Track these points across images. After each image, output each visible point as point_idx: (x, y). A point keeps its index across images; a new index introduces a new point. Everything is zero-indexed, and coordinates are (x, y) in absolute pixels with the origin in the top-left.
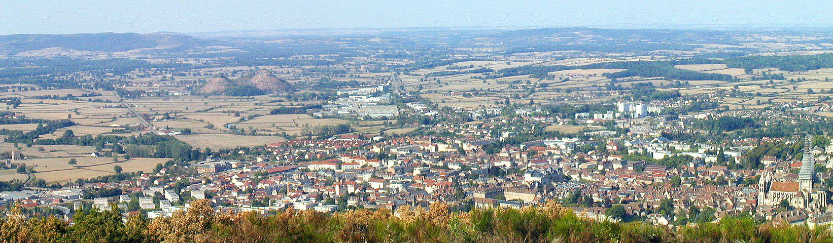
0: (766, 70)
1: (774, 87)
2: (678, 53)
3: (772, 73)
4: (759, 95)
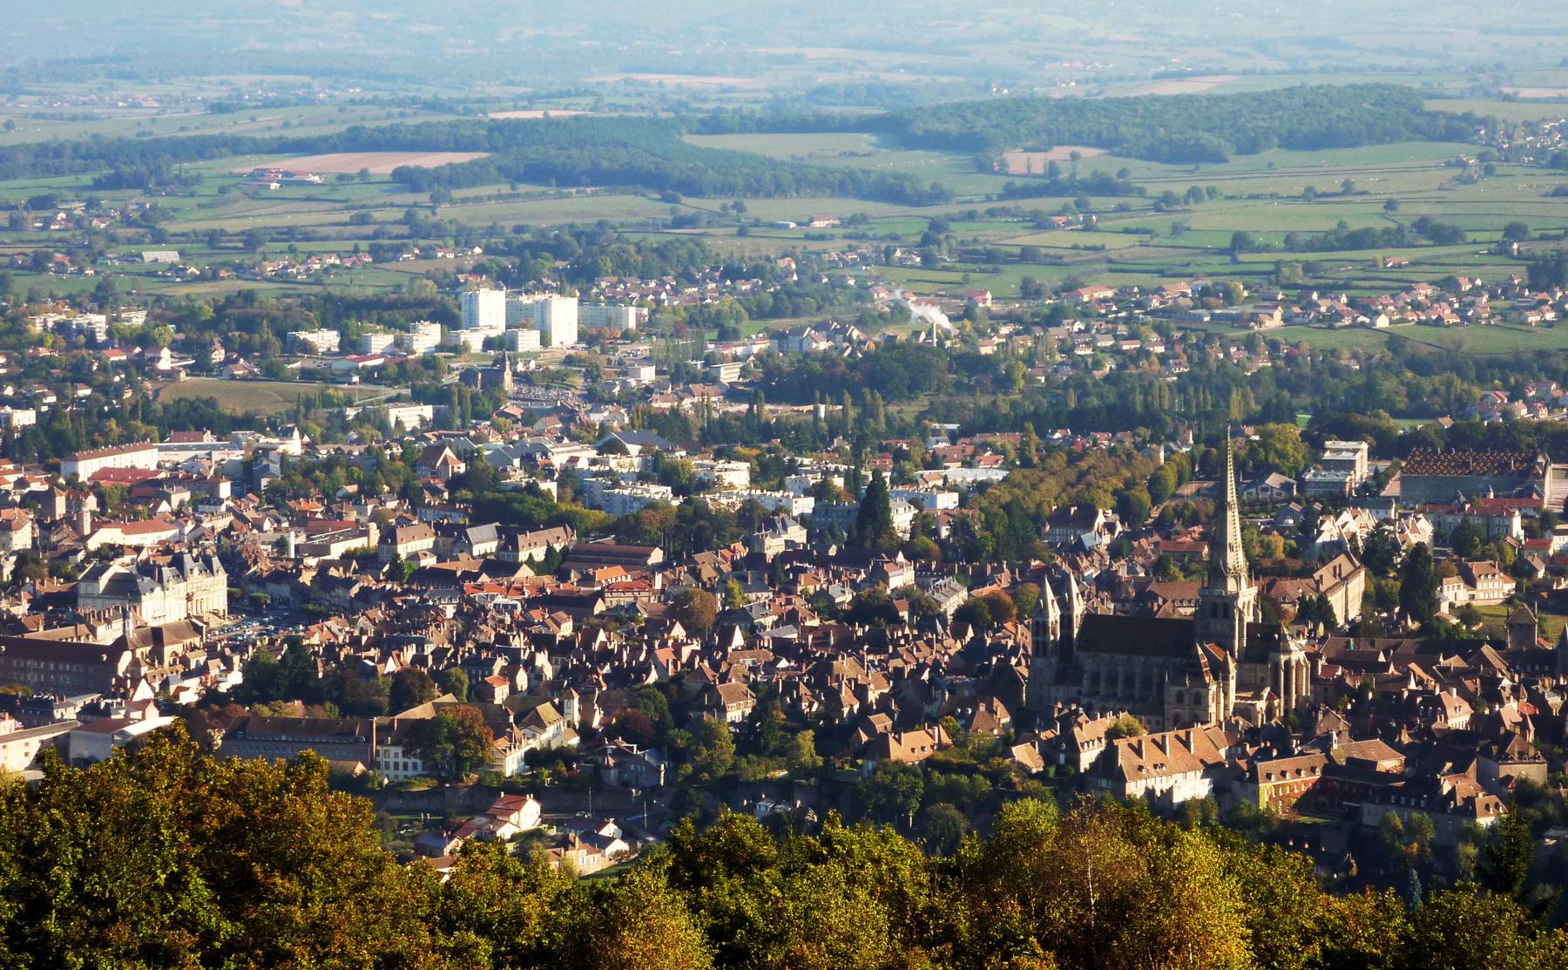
0: (1060, 153)
1: (1088, 228)
2: (670, 80)
3: (1084, 173)
4: (1028, 255)
